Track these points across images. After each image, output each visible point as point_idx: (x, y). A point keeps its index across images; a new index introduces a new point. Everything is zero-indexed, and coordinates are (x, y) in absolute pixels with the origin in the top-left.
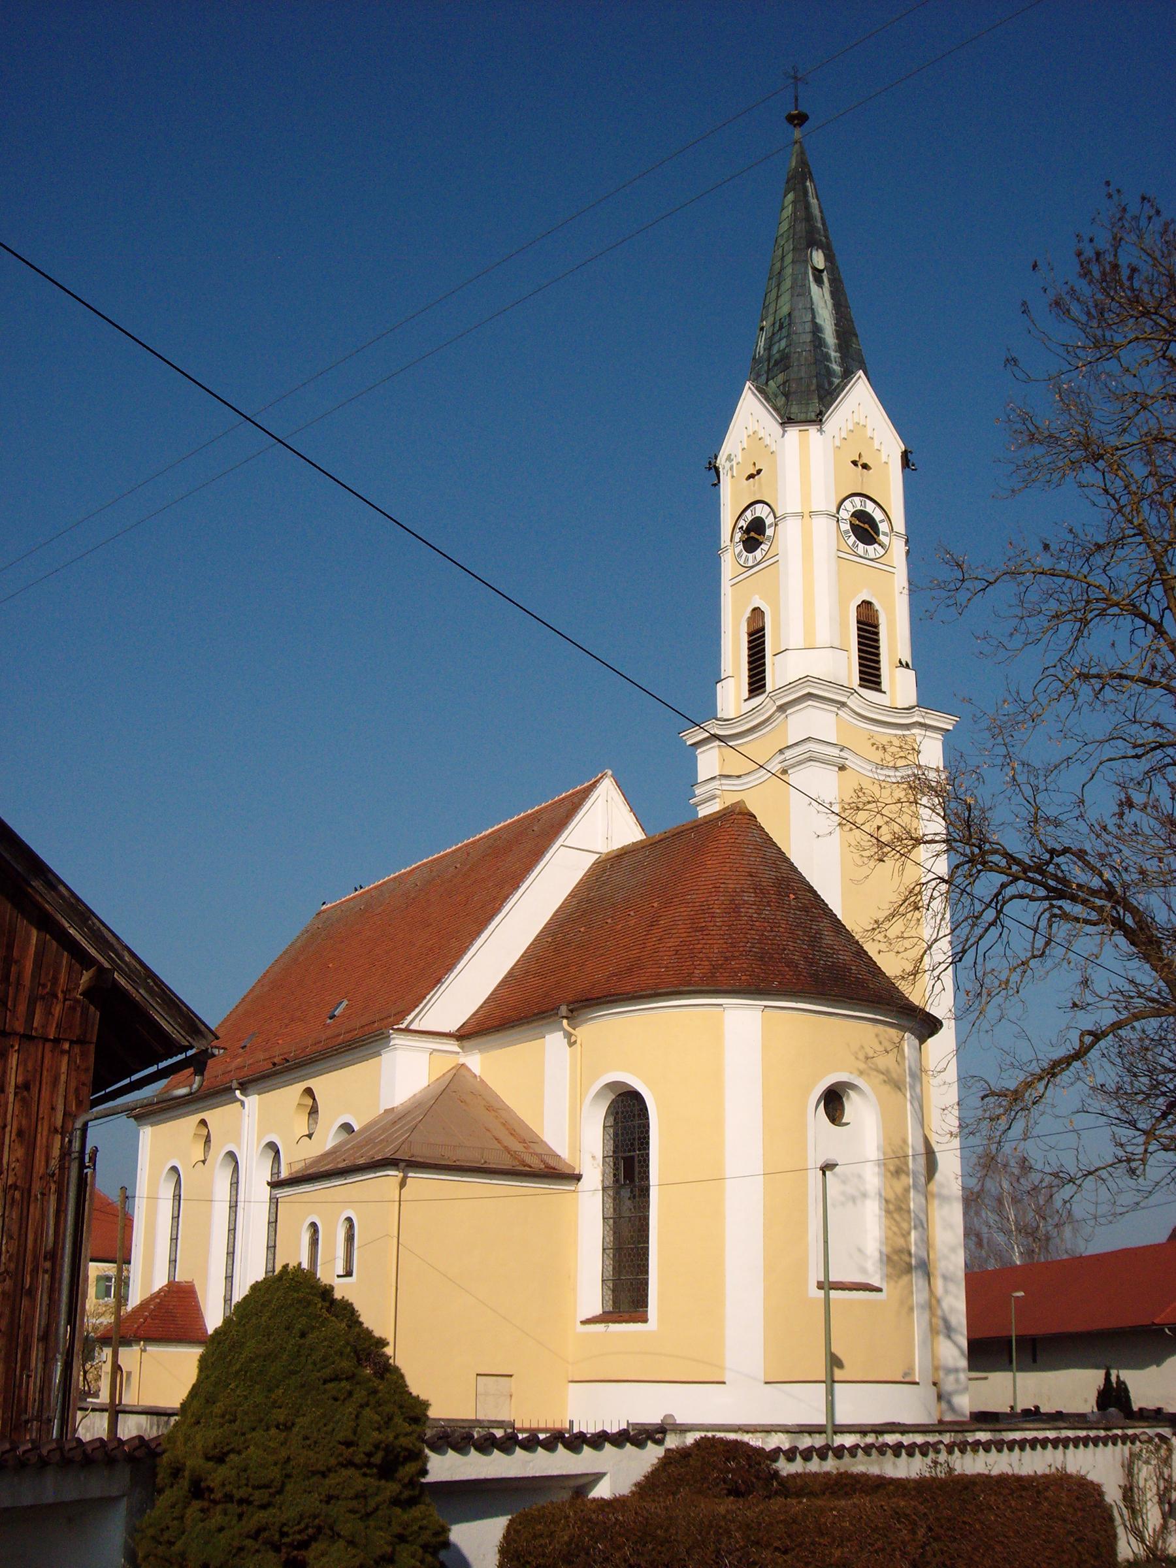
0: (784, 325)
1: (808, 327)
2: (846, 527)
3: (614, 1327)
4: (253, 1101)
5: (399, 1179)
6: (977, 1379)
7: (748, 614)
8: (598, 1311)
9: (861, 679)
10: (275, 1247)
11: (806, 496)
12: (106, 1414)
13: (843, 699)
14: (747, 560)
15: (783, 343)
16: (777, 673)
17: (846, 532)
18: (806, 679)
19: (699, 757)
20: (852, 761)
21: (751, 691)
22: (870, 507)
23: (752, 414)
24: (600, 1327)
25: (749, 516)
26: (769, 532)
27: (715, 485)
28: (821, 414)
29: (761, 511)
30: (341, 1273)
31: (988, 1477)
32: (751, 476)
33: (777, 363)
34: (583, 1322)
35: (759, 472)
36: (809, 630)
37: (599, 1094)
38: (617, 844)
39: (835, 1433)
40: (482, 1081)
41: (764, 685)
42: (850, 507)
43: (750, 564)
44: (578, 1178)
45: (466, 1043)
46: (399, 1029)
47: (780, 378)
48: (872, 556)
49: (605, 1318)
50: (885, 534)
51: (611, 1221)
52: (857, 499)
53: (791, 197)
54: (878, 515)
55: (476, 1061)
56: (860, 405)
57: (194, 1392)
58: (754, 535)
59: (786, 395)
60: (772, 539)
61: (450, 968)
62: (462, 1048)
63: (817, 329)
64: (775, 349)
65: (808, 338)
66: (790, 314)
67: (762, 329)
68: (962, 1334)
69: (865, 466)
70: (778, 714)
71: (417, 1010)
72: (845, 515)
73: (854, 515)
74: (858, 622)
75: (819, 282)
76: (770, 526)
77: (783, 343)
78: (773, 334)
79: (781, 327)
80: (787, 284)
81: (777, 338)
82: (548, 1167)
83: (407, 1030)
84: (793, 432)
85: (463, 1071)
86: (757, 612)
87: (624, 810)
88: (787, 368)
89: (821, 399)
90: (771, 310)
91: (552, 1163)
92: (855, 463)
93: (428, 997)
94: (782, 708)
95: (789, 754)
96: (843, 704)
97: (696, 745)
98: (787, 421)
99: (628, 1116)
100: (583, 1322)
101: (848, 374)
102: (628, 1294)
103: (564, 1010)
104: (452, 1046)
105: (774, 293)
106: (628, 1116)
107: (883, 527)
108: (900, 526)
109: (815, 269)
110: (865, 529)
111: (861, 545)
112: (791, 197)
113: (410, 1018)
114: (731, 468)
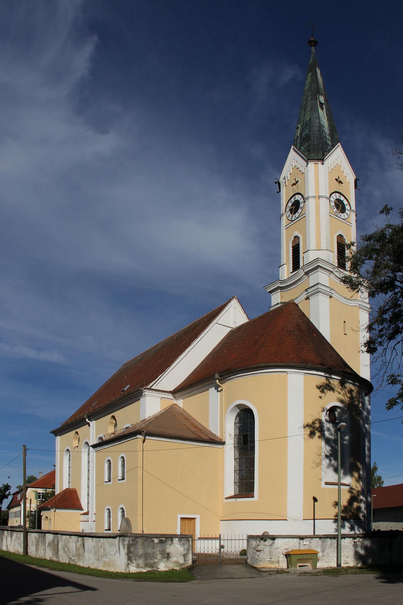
0: (308, 125)
1: (317, 124)
3: (239, 500)
4: (93, 424)
5: (143, 440)
7: (292, 239)
8: (232, 494)
11: (317, 190)
12: (22, 533)
13: (332, 270)
15: (307, 131)
16: (306, 258)
17: (333, 206)
18: (317, 260)
20: (335, 295)
21: (293, 269)
22: (342, 198)
23: (293, 158)
24: (234, 500)
25: (293, 200)
26: (301, 205)
27: (278, 192)
28: (324, 156)
29: (298, 197)
30: (120, 478)
31: (45, 559)
32: (294, 184)
33: (304, 139)
34: (226, 498)
35: (297, 182)
36: (318, 243)
37: (232, 410)
38: (239, 324)
39: (342, 538)
40: (183, 409)
42: (335, 196)
44: (223, 443)
45: (176, 395)
46: (147, 388)
47: (306, 145)
50: (348, 210)
51: (238, 460)
52: (337, 194)
53: (310, 74)
54: (345, 202)
55: (180, 403)
56: (337, 156)
58: (295, 207)
59: (309, 151)
60: (302, 208)
61: (169, 365)
62: (175, 397)
63: (321, 126)
64: (304, 134)
65: (318, 129)
66: (310, 120)
67: (298, 128)
69: (340, 182)
70: (305, 276)
71: (154, 381)
73: (337, 200)
75: (322, 109)
76: (302, 203)
77: (307, 131)
78: (303, 129)
79: (306, 125)
80: (309, 108)
81: (304, 130)
82: (211, 439)
83: (150, 389)
84: (311, 164)
85: (175, 406)
86: (296, 237)
87: (242, 312)
88: (309, 140)
89: (323, 153)
90: (302, 120)
91: (212, 437)
92: (336, 180)
93: (159, 377)
94: (307, 273)
95: (309, 290)
96: (332, 272)
97: (271, 292)
98: (308, 160)
99: (246, 417)
100: (226, 498)
101: (333, 146)
102: (246, 486)
103: (217, 376)
104: (170, 396)
105: (303, 114)
106: (246, 417)
107: (347, 207)
108: (353, 208)
109: (320, 102)
110: (340, 206)
112: (310, 74)
113: (151, 384)
114: (285, 183)
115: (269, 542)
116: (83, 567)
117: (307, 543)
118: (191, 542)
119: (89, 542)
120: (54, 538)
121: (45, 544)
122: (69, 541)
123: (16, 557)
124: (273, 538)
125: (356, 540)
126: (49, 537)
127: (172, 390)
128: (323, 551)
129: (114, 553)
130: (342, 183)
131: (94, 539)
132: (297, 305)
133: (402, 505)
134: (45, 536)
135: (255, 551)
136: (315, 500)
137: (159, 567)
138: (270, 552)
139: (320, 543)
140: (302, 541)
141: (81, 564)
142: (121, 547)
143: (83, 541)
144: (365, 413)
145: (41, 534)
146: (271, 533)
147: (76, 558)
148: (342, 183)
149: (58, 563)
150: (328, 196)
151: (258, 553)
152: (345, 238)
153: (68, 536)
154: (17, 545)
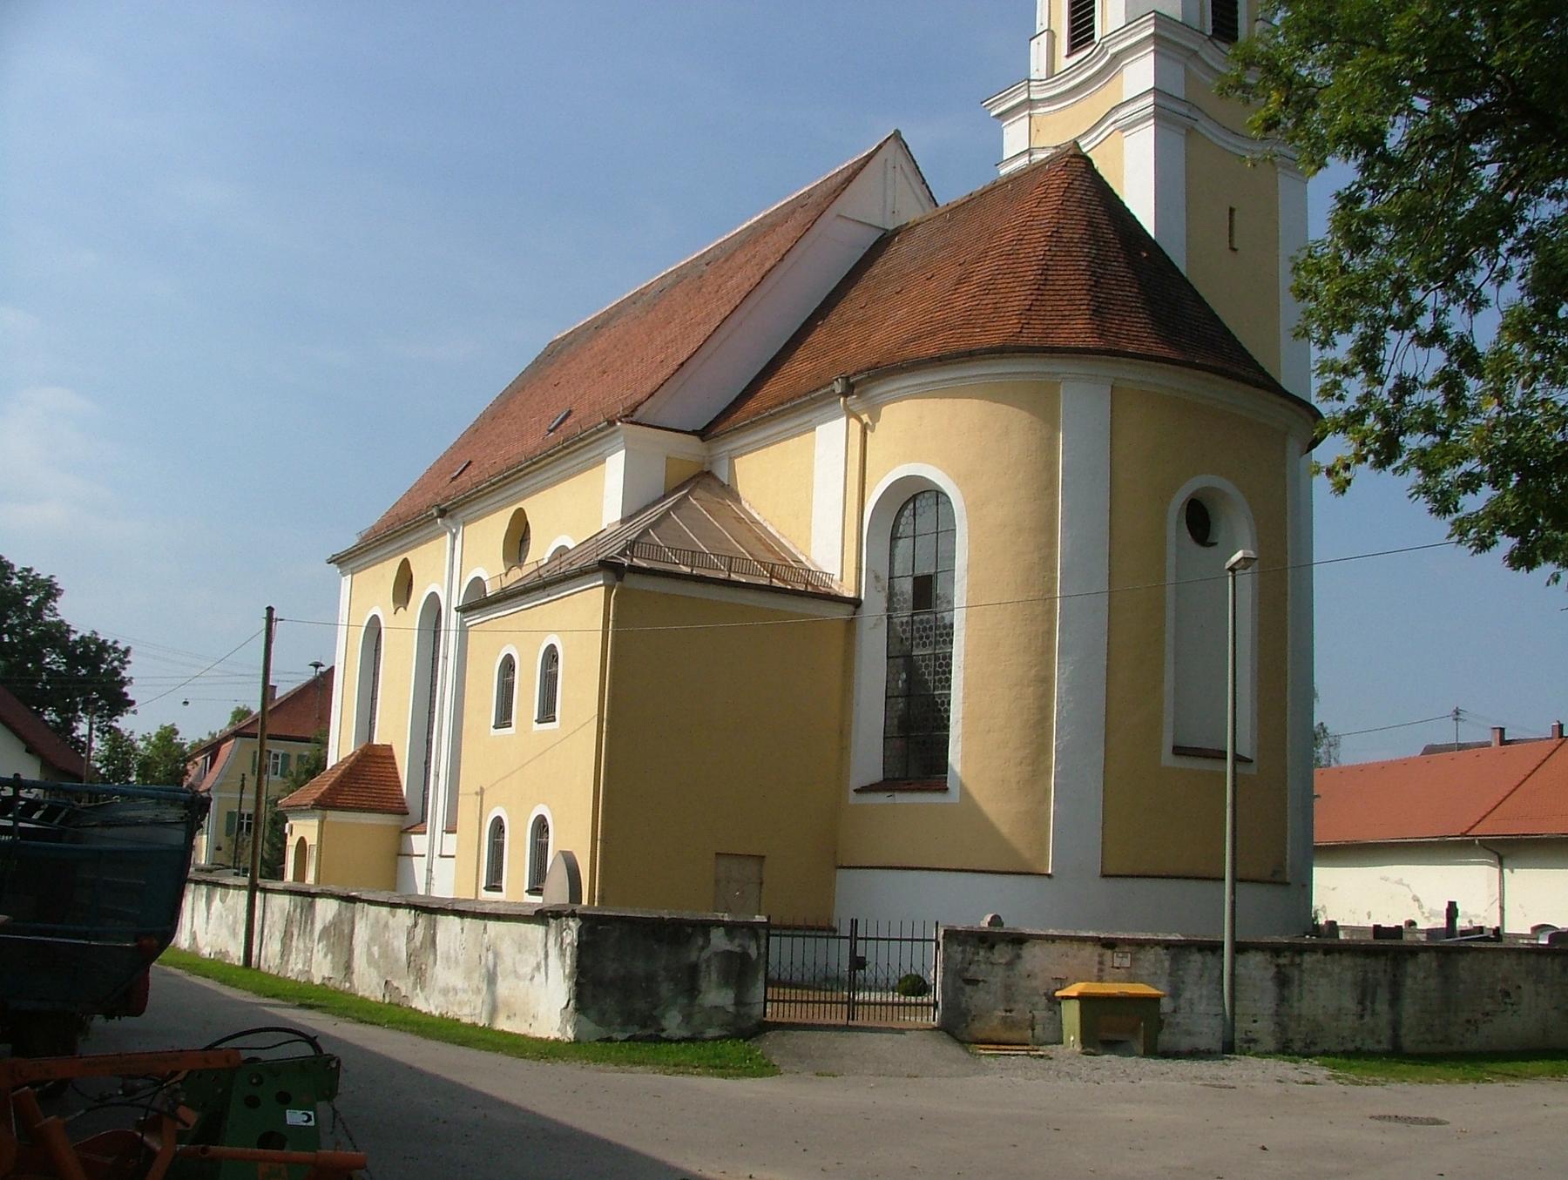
3: (902, 799)
20: (1203, 126)
24: (881, 798)
49: (889, 784)
104: (695, 439)
115: (1002, 954)
116: (428, 1015)
117: (1127, 962)
118: (763, 942)
119: (448, 928)
120: (339, 913)
121: (312, 931)
122: (386, 925)
123: (636, 1055)
124: (1019, 940)
125: (1282, 961)
126: (326, 910)
128: (1175, 993)
129: (528, 970)
131: (468, 921)
132: (1090, 160)
133: (1315, 869)
134: (312, 906)
135: (960, 983)
137: (665, 1023)
138: (1007, 987)
139: (1167, 964)
140: (1109, 952)
141: (421, 1003)
142: (553, 952)
143: (432, 928)
145: (299, 899)
146: (1010, 924)
147: (404, 985)
149: (350, 995)
151: (968, 988)
153: (385, 910)
154: (225, 932)
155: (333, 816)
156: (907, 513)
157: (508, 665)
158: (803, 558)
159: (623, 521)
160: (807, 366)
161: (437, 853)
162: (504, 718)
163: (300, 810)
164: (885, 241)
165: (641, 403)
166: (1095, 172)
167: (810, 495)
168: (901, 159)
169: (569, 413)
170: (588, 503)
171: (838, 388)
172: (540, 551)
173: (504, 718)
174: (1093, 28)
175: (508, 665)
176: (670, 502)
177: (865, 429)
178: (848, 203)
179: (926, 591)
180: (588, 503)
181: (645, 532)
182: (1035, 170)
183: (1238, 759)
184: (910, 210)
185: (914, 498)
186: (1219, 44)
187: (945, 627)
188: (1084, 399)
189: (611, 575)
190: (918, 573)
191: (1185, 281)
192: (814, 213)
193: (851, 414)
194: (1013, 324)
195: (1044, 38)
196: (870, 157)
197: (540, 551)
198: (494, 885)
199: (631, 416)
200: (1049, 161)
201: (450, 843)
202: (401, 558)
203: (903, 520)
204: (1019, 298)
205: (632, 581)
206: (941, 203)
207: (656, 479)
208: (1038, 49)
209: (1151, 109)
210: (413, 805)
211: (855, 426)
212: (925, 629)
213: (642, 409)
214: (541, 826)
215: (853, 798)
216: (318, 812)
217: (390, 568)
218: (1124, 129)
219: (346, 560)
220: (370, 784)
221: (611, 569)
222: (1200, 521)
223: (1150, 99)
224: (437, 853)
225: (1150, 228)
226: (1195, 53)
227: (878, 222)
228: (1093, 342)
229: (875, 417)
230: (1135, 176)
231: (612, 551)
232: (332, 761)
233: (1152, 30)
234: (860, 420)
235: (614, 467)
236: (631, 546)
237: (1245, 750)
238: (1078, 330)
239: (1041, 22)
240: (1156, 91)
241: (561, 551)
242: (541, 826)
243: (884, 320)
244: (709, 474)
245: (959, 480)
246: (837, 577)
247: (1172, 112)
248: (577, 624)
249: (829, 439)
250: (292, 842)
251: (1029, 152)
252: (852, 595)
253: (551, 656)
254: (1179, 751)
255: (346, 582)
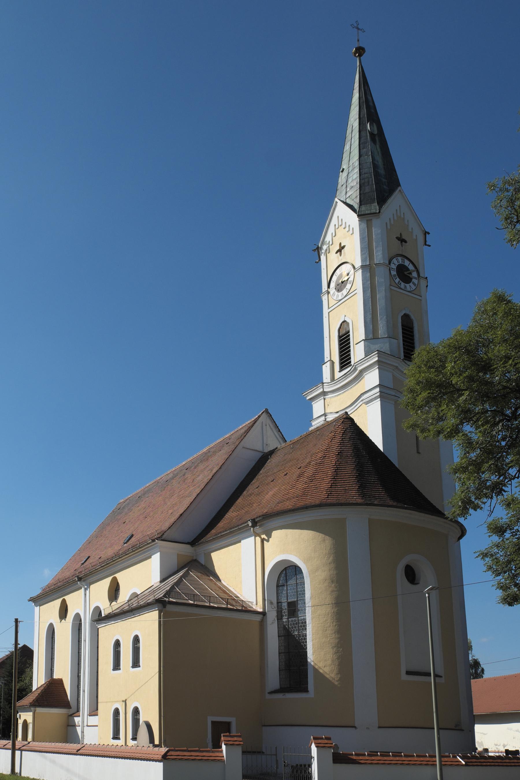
2: (394, 273)
6: (277, 438)
9: (405, 356)
10: (278, 586)
14: (338, 296)
17: (394, 275)
19: (314, 406)
22: (407, 263)
24: (280, 696)
41: (350, 362)
42: (396, 262)
43: (340, 298)
48: (409, 289)
49: (282, 690)
52: (400, 258)
57: (25, 777)
68: (478, 742)
72: (393, 266)
74: (402, 325)
97: (313, 399)
100: (271, 693)
104: (188, 546)
111: (403, 284)
127: (190, 541)
130: (406, 242)
132: (353, 420)
133: (476, 725)
136: (418, 453)
144: (485, 399)
148: (406, 242)
150: (388, 263)
152: (412, 317)
155: (39, 710)
156: (283, 575)
157: (117, 644)
158: (239, 596)
159: (161, 581)
160: (235, 514)
161: (85, 724)
162: (117, 666)
163: (25, 709)
164: (264, 458)
165: (165, 532)
166: (356, 424)
167: (241, 568)
168: (269, 421)
169: (132, 536)
170: (144, 576)
171: (250, 524)
172: (124, 597)
173: (117, 666)
174: (350, 358)
175: (117, 644)
176: (181, 574)
177: (263, 541)
178: (249, 441)
179: (294, 608)
180: (144, 576)
181: (172, 588)
182: (327, 425)
183: (436, 676)
184: (272, 443)
185: (285, 569)
186: (406, 361)
187: (302, 623)
188: (357, 522)
189: (160, 605)
190: (289, 600)
191: (398, 470)
192: (233, 447)
193: (256, 535)
194: (324, 495)
195: (328, 364)
196: (255, 421)
197: (124, 597)
198: (116, 737)
199: (162, 537)
200: (335, 420)
201: (93, 720)
202: (62, 599)
203: (282, 579)
204: (325, 485)
205: (169, 608)
206: (288, 441)
207: (174, 563)
208: (326, 369)
209: (378, 394)
210: (73, 704)
211: (258, 539)
212: (294, 624)
213: (166, 534)
214: (136, 711)
215: (268, 697)
216: (32, 709)
217: (57, 603)
218: (367, 403)
219: (40, 600)
220: (53, 694)
221: (159, 601)
222: (411, 574)
223: (378, 390)
224: (85, 724)
225: (380, 447)
226: (397, 367)
227: (260, 449)
228: (360, 501)
229: (269, 536)
230: (371, 423)
231: (160, 595)
232: (34, 688)
233: (377, 359)
234: (260, 537)
235: (156, 559)
236: (168, 594)
237: (440, 671)
238: (354, 495)
239: (327, 358)
240: (380, 385)
241: (135, 595)
242: (136, 711)
243: (268, 493)
244: (196, 561)
245: (306, 561)
246: (255, 603)
247: (387, 393)
248: (147, 626)
249: (248, 546)
250: (20, 722)
251: (325, 415)
252: (261, 610)
253: (136, 640)
254: (408, 673)
255: (37, 609)
